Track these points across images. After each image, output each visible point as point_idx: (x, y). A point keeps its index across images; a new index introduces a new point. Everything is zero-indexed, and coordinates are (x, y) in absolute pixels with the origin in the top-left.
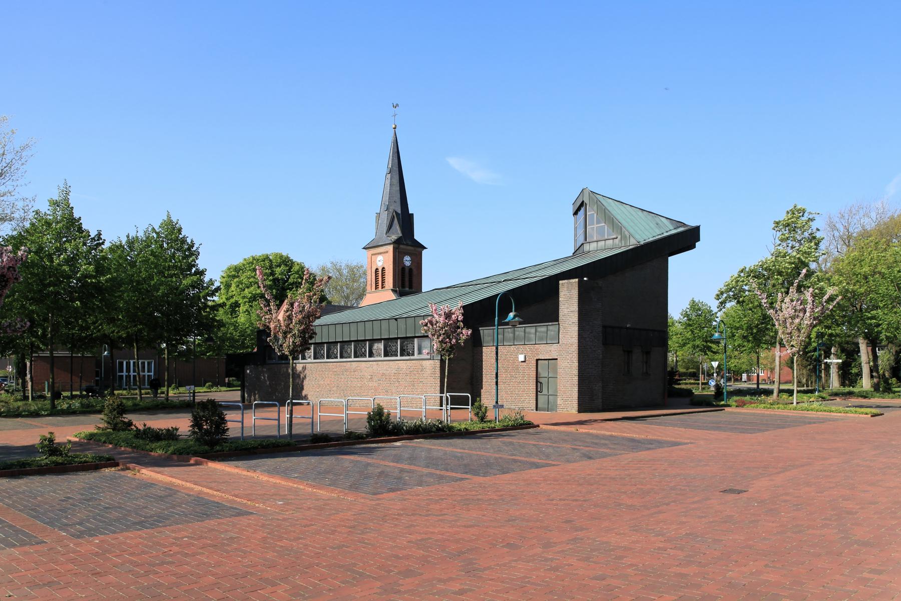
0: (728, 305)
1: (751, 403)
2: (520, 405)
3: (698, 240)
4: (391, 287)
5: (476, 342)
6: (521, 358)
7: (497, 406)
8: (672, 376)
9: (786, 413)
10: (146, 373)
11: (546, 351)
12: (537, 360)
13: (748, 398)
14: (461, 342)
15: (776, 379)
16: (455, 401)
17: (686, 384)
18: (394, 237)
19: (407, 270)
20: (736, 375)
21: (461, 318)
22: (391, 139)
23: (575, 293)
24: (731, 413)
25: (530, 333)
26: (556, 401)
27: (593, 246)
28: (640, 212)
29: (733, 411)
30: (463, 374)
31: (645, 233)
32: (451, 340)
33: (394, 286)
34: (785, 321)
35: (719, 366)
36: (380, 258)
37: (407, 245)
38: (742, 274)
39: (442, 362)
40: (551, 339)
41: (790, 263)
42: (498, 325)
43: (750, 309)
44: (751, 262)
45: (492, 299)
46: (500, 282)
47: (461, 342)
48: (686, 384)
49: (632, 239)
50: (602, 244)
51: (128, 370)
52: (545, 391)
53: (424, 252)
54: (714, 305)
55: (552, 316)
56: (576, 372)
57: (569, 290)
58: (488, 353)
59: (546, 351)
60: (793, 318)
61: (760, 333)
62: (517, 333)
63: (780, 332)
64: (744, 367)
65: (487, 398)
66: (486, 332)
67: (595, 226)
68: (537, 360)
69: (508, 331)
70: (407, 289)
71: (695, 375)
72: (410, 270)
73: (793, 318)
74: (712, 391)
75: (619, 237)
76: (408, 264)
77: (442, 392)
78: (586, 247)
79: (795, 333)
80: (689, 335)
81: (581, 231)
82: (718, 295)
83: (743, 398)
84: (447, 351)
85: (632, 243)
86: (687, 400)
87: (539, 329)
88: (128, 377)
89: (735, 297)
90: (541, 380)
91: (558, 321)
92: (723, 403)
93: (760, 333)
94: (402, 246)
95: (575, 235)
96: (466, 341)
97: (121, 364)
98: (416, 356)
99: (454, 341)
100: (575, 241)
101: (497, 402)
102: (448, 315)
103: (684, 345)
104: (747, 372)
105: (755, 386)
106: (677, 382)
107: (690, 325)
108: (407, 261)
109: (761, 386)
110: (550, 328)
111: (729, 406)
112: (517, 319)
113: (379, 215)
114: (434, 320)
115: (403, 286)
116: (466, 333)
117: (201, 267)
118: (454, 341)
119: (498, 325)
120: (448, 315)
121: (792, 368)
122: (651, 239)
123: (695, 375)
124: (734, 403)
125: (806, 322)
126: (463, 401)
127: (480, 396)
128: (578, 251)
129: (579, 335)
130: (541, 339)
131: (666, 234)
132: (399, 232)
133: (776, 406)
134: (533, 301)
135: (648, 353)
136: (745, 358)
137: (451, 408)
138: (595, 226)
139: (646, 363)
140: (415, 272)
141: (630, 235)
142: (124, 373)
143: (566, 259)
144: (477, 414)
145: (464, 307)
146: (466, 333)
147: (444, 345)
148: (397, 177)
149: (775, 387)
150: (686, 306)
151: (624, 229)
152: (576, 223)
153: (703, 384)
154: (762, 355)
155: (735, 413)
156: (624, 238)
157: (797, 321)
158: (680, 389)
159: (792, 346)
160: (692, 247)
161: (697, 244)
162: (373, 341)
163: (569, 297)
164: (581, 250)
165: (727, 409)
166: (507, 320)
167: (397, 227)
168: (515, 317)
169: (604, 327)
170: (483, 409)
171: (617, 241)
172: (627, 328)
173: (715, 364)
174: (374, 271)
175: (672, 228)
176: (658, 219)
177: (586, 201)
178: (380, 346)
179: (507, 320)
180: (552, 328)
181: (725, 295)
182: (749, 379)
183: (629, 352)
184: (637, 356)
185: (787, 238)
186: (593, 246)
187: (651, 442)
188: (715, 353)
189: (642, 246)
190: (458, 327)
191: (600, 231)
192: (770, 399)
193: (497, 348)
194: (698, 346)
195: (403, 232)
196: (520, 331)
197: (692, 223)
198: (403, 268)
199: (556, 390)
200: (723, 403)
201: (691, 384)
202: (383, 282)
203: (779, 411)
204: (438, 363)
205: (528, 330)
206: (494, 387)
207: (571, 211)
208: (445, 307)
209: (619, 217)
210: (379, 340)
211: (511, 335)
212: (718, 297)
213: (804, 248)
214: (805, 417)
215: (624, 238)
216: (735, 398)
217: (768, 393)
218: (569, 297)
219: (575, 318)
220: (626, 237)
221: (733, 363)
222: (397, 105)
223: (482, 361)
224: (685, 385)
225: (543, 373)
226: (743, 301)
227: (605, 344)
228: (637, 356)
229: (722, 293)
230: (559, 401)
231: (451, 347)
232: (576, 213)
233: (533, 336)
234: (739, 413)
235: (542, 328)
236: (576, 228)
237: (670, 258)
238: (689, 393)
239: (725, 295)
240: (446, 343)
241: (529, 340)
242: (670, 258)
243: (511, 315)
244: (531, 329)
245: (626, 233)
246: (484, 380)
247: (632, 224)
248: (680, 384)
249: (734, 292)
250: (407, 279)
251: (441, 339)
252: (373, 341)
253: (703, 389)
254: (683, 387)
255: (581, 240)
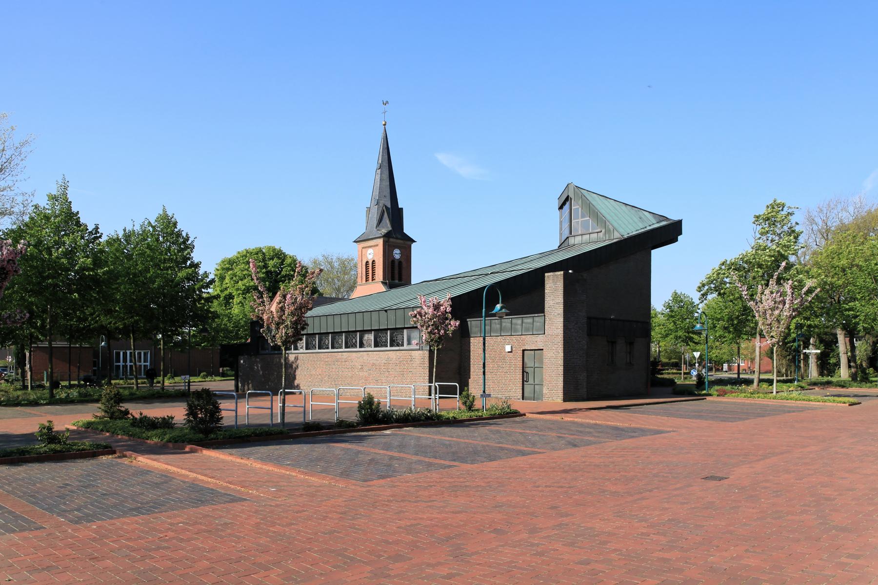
0: (710, 297)
1: (732, 392)
2: (507, 394)
3: (681, 233)
4: (381, 279)
5: (464, 333)
6: (508, 348)
7: (485, 395)
8: (655, 366)
9: (766, 402)
10: (143, 363)
11: (532, 342)
12: (524, 351)
13: (729, 387)
14: (450, 333)
15: (756, 369)
16: (444, 390)
17: (669, 374)
18: (384, 231)
19: (397, 263)
20: (717, 365)
21: (449, 309)
22: (381, 135)
23: (560, 285)
24: (712, 402)
25: (516, 324)
26: (541, 391)
27: (578, 240)
28: (624, 207)
29: (714, 400)
30: (451, 364)
31: (628, 227)
32: (439, 331)
33: (384, 278)
34: (765, 313)
35: (700, 356)
36: (370, 251)
37: (397, 238)
38: (723, 267)
39: (431, 352)
40: (537, 330)
41: (770, 256)
42: (486, 316)
43: (731, 301)
44: (732, 255)
45: (479, 291)
46: (487, 275)
47: (450, 333)
48: (669, 374)
49: (616, 232)
50: (586, 237)
51: (125, 360)
52: (531, 381)
53: (413, 245)
54: (695, 297)
55: (538, 308)
56: (561, 362)
57: (555, 282)
58: (475, 344)
59: (532, 342)
60: (773, 309)
61: (740, 324)
62: (504, 324)
63: (760, 323)
64: (725, 357)
65: (475, 388)
66: (473, 324)
67: (580, 220)
68: (524, 351)
69: (495, 323)
70: (397, 281)
71: (677, 365)
72: (400, 262)
73: (773, 309)
74: (693, 380)
75: (603, 231)
76: (397, 257)
77: (431, 381)
78: (572, 241)
79: (775, 324)
80: (671, 326)
81: (566, 225)
82: (699, 287)
83: (724, 387)
84: (436, 341)
85: (616, 237)
86: (670, 389)
87: (525, 320)
88: (125, 367)
89: (717, 289)
90: (527, 370)
91: (543, 312)
92: (704, 392)
93: (740, 324)
94: (391, 240)
95: (561, 229)
96: (454, 332)
97: (118, 354)
98: (405, 347)
99: (442, 332)
100: (561, 234)
101: (484, 392)
102: (437, 307)
103: (667, 336)
104: (728, 362)
105: (736, 376)
106: (660, 372)
107: (672, 317)
108: (397, 254)
109: (741, 376)
110: (536, 319)
111: (710, 395)
112: (503, 310)
113: (369, 209)
114: (423, 312)
115: (393, 278)
116: (454, 324)
117: (196, 260)
118: (442, 332)
119: (486, 316)
120: (437, 307)
121: (772, 358)
122: (635, 233)
123: (677, 365)
124: (715, 393)
125: (785, 314)
126: (451, 391)
127: (467, 385)
128: (564, 244)
129: (564, 326)
130: (527, 330)
131: (649, 228)
132: (389, 225)
133: (756, 396)
134: (519, 293)
135: (631, 344)
136: (726, 348)
137: (440, 398)
138: (580, 220)
139: (630, 353)
140: (404, 264)
141: (614, 229)
142: (121, 364)
143: (552, 252)
144: (465, 403)
145: (452, 299)
146: (454, 324)
147: (433, 336)
148: (387, 173)
149: (755, 377)
150: (668, 297)
151: (608, 223)
152: (561, 217)
153: (685, 373)
154: (743, 345)
155: (716, 402)
156: (608, 231)
157: (777, 312)
158: (663, 379)
159: (772, 337)
160: (675, 240)
161: (679, 237)
162: (363, 332)
163: (554, 289)
164: (566, 244)
165: (708, 398)
166: (494, 312)
167: (386, 221)
168: (502, 308)
169: (589, 318)
170: (471, 399)
171: (601, 235)
172: (611, 320)
173: (697, 355)
174: (364, 264)
175: (654, 222)
176: (641, 213)
177: (571, 195)
178: (371, 337)
179: (494, 312)
180: (538, 319)
181: (706, 287)
182: (730, 368)
183: (613, 343)
184: (621, 346)
185: (767, 232)
186: (578, 240)
187: (634, 430)
188: (696, 343)
189: (626, 240)
190: (447, 319)
191: (585, 225)
192: (751, 389)
193: (484, 339)
194: (680, 337)
195: (392, 226)
196: (506, 322)
197: (675, 217)
198: (393, 261)
199: (542, 380)
200: (704, 392)
201: (673, 373)
202: (373, 274)
203: (760, 400)
204: (427, 353)
205: (514, 321)
206: (482, 377)
207: (556, 205)
208: (434, 299)
209: (603, 212)
210: (370, 331)
211: (498, 326)
212: (700, 289)
213: (784, 242)
214: (785, 406)
215: (608, 231)
216: (716, 387)
217: (749, 382)
218: (554, 289)
219: (560, 309)
220: (610, 230)
221: (714, 354)
222: (387, 102)
223: (470, 352)
224: (667, 374)
225: (529, 363)
226: (724, 293)
227: (590, 334)
228: (621, 346)
229: (704, 285)
230: (545, 391)
231: (439, 338)
232: (561, 208)
233: (519, 327)
234: (720, 402)
235: (528, 320)
236: (561, 222)
237: (653, 251)
238: (671, 382)
239: (706, 287)
240: (434, 334)
241: (516, 331)
242: (653, 251)
243: (498, 306)
244: (517, 321)
245: (610, 226)
246: (472, 370)
247: (616, 218)
248: (662, 374)
249: (715, 284)
250: (396, 272)
251: (429, 330)
252: (363, 332)
253: (685, 378)
254: (666, 376)
255: (566, 233)
